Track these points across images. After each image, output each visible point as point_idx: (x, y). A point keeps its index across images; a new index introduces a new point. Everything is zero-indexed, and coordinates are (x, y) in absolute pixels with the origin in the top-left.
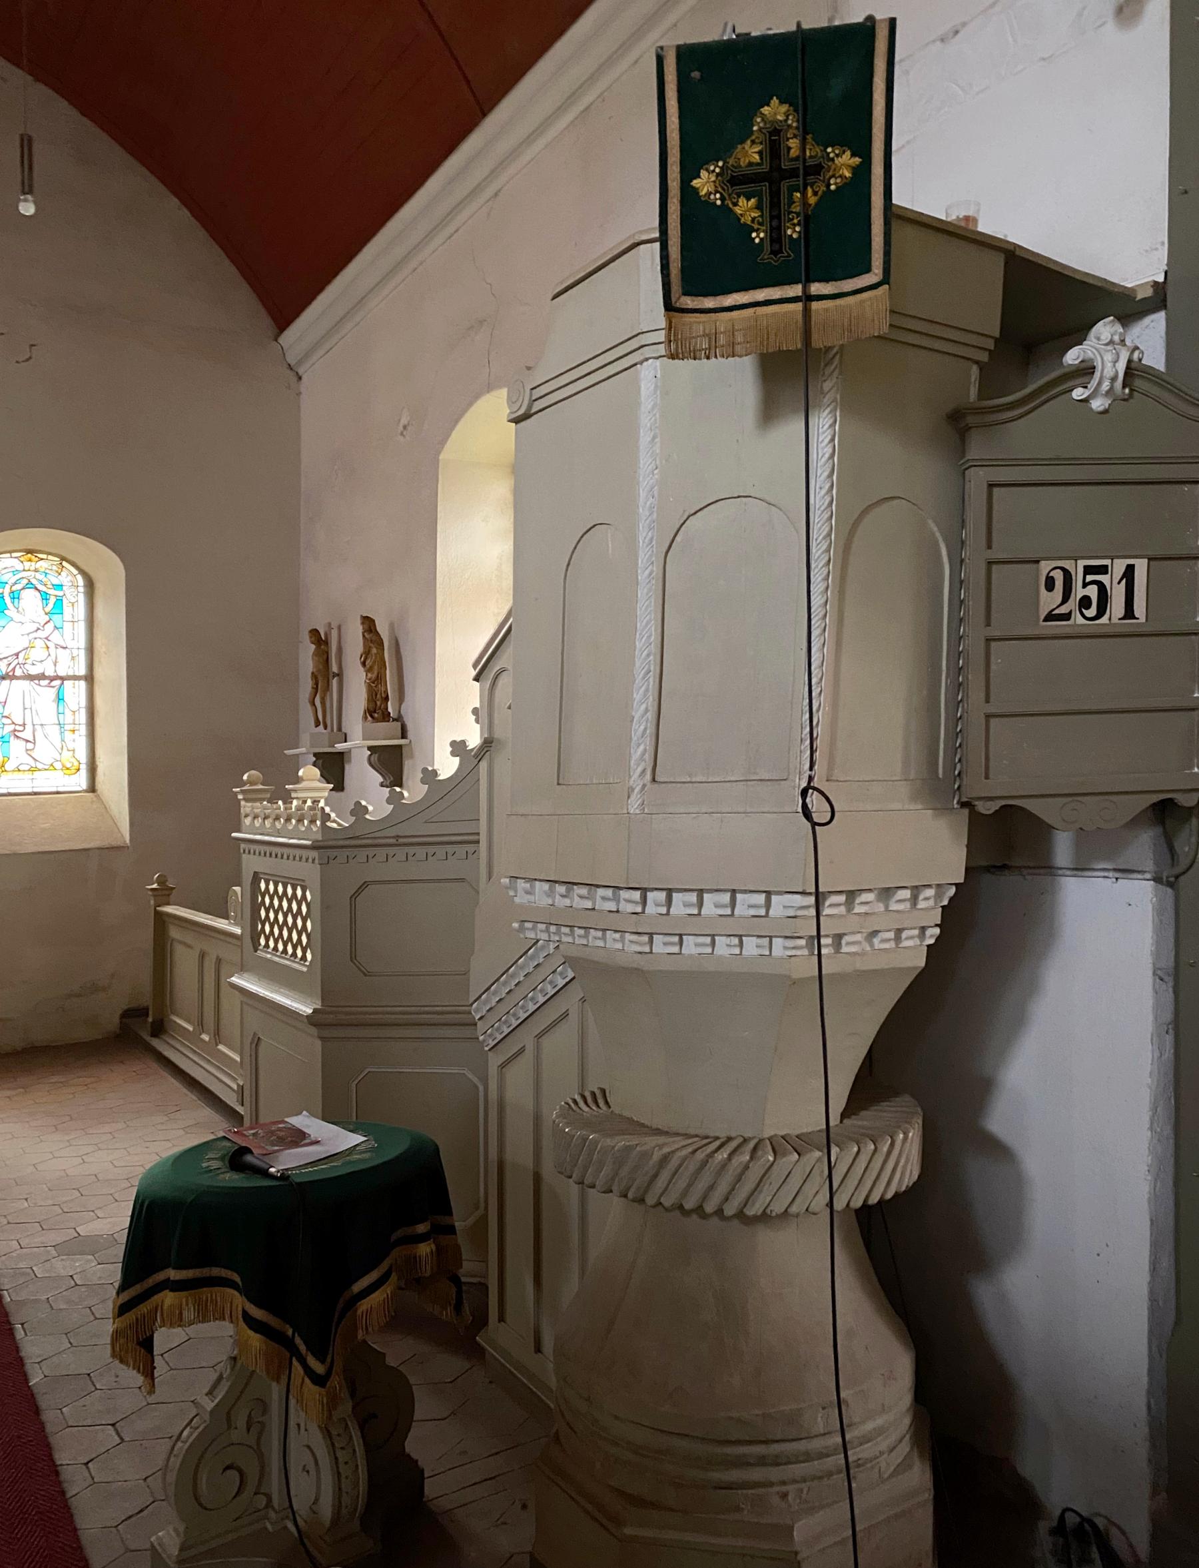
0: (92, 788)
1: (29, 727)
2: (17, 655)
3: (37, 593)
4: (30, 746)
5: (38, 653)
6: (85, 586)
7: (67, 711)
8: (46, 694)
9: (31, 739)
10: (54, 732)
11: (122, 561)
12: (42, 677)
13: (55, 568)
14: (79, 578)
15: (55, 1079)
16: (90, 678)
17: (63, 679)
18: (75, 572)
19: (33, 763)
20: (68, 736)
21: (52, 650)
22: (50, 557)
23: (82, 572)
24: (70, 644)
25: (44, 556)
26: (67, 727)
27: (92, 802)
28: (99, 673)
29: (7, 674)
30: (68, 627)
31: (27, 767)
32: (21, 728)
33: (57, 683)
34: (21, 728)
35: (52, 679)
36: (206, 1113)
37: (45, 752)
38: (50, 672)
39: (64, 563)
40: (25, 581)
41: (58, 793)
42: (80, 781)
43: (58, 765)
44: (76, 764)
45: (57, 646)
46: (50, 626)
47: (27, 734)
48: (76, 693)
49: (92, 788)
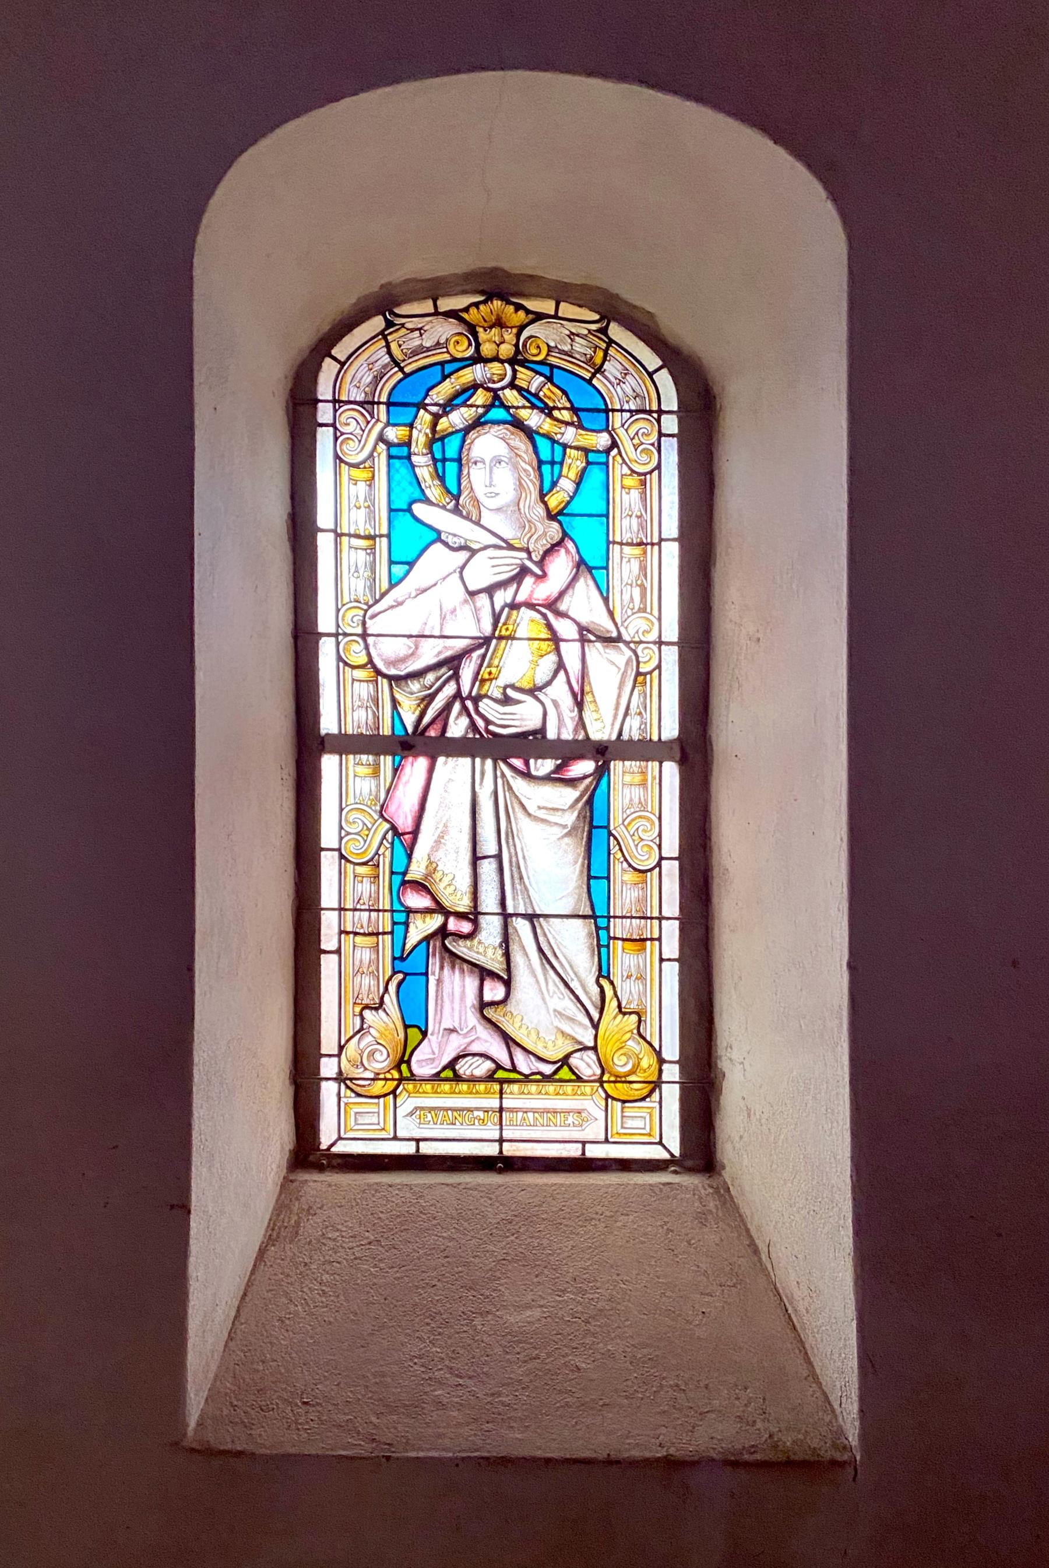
0: (701, 1150)
1: (491, 927)
2: (453, 663)
3: (520, 442)
4: (494, 991)
5: (517, 662)
6: (683, 412)
7: (618, 868)
8: (547, 805)
9: (496, 964)
10: (572, 940)
11: (835, 196)
12: (530, 743)
13: (580, 346)
14: (664, 379)
15: (724, 520)
16: (694, 750)
17: (603, 753)
18: (652, 361)
19: (500, 1053)
20: (623, 960)
21: (571, 652)
22: (567, 310)
23: (677, 359)
24: (634, 627)
25: (547, 306)
26: (618, 928)
27: (702, 1218)
28: (733, 726)
29: (420, 731)
30: (625, 567)
31: (483, 1067)
32: (466, 927)
33: (585, 767)
34: (466, 927)
35: (568, 752)
36: (453, 437)
37: (542, 1014)
38: (561, 728)
39: (616, 331)
40: (481, 398)
41: (583, 1165)
42: (656, 1127)
43: (585, 1064)
44: (648, 1061)
45: (585, 634)
46: (560, 567)
47: (485, 948)
48: (647, 803)
49: (701, 1150)
